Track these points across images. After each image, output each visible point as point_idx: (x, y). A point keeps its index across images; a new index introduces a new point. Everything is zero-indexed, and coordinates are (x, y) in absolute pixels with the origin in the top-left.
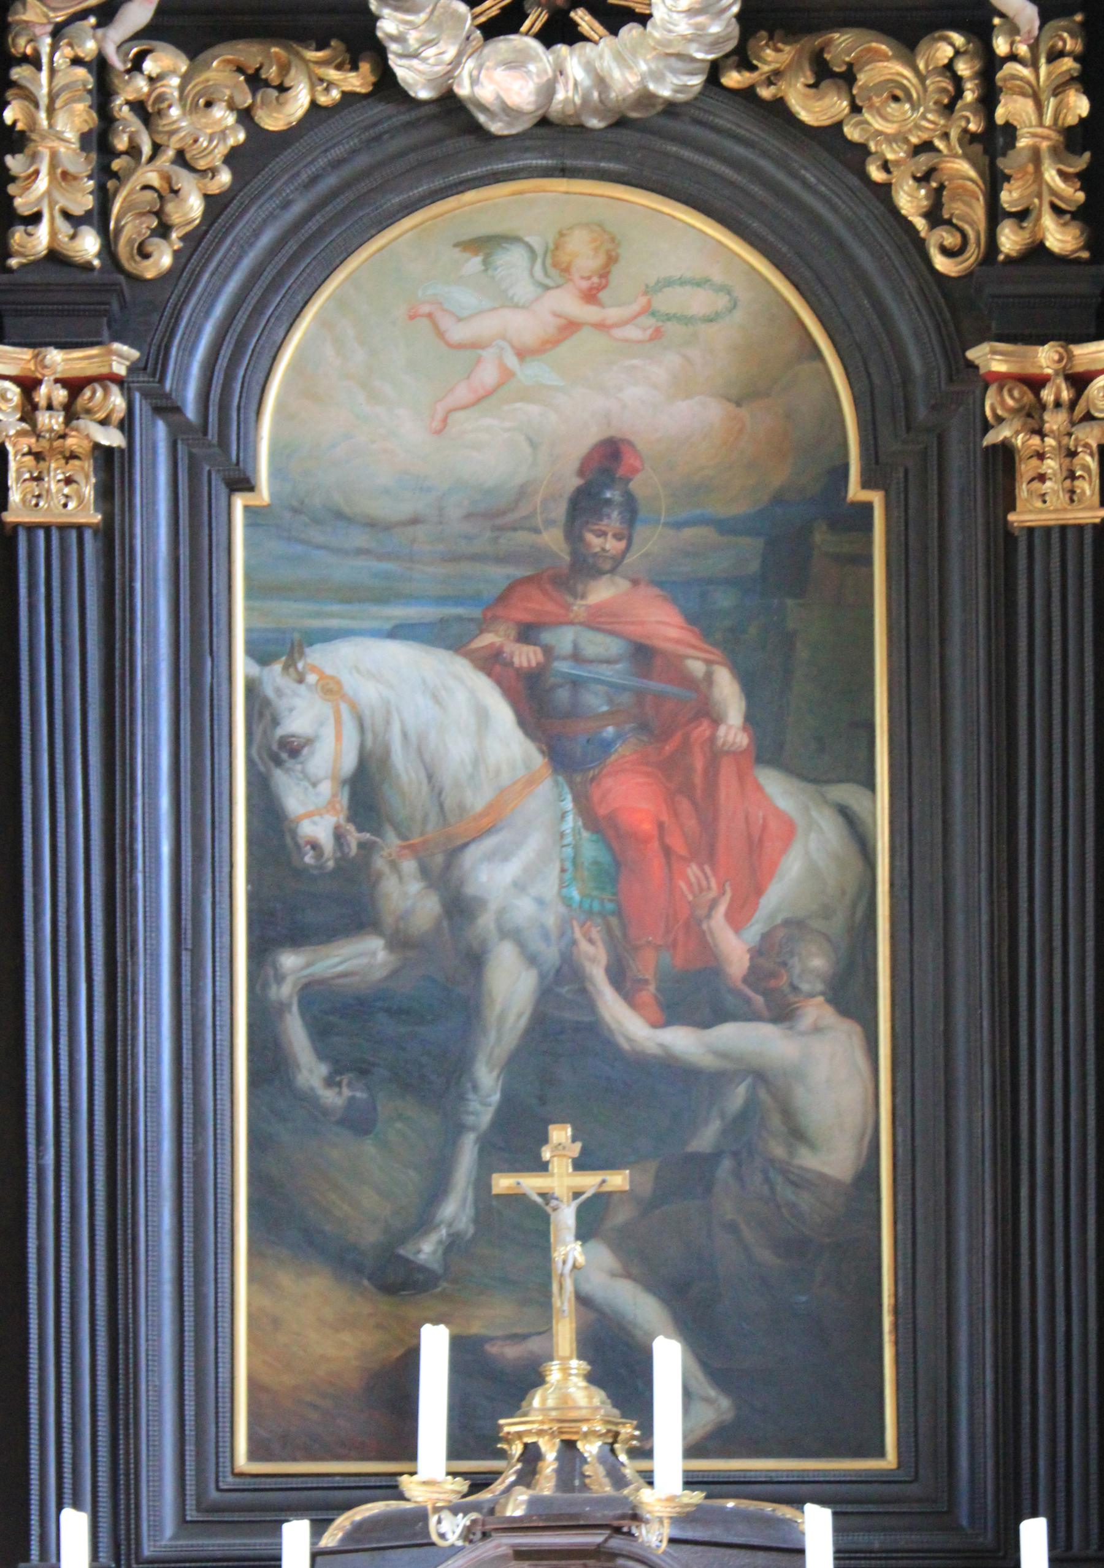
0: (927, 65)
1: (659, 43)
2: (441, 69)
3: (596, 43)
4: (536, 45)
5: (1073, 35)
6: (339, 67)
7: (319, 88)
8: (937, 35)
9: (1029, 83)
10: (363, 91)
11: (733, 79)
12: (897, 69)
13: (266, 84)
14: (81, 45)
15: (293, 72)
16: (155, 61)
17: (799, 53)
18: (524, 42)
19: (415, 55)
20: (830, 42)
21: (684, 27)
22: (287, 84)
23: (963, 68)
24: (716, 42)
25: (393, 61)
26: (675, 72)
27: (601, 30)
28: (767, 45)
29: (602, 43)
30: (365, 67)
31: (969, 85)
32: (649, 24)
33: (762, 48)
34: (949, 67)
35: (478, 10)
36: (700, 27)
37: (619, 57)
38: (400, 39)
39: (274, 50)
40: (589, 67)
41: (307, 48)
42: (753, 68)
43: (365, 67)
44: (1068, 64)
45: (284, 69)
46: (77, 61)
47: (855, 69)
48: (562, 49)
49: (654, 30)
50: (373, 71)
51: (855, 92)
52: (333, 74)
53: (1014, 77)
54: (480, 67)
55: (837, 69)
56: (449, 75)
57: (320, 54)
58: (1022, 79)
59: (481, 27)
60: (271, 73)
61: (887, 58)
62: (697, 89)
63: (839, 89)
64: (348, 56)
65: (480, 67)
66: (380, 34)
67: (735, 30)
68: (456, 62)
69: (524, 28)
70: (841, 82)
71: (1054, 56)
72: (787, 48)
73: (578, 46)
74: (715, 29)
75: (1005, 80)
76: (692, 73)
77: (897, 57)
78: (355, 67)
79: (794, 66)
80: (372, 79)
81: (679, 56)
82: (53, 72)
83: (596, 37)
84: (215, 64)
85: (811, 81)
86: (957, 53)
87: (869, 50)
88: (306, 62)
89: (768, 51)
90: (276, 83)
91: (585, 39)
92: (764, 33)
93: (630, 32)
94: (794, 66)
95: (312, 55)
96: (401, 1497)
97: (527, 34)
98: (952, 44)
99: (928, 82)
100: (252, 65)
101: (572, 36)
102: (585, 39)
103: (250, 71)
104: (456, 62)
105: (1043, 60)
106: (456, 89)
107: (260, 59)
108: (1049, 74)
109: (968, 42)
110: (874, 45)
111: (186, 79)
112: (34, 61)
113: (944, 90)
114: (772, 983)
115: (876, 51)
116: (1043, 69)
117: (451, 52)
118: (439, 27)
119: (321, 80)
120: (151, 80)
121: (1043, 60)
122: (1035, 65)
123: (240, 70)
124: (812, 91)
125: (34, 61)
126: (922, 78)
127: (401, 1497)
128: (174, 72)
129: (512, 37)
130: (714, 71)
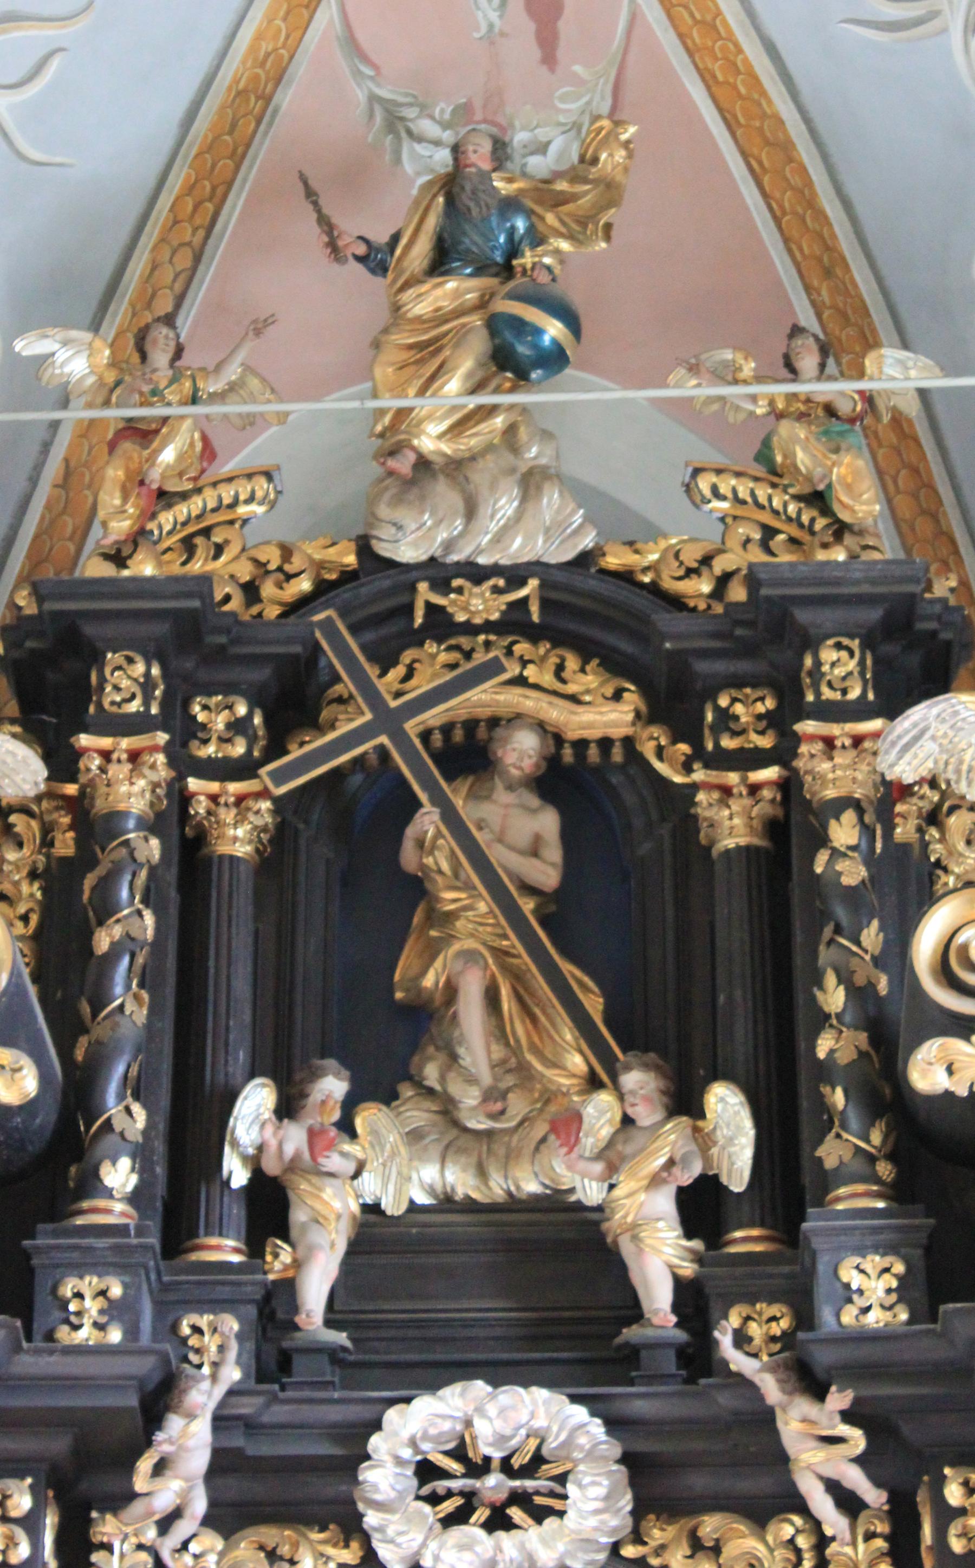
0: (775, 1540)
1: (573, 1531)
2: (411, 1551)
3: (526, 1530)
4: (481, 1533)
5: (881, 1520)
6: (335, 1545)
7: (320, 1562)
8: (782, 1516)
9: (851, 1559)
10: (353, 1563)
11: (629, 1551)
12: (752, 1544)
13: (281, 1558)
14: (144, 1534)
15: (301, 1549)
16: (199, 1542)
17: (681, 1529)
18: (472, 1531)
19: (392, 1541)
20: (703, 1521)
21: (593, 1522)
22: (296, 1559)
23: (802, 1542)
24: (615, 1530)
25: (376, 1544)
26: (586, 1551)
27: (530, 1521)
28: (654, 1526)
29: (531, 1531)
30: (355, 1545)
31: (807, 1555)
32: (565, 1517)
33: (651, 1528)
34: (792, 1541)
35: (439, 1508)
36: (603, 1522)
37: (544, 1542)
38: (381, 1529)
39: (287, 1533)
40: (522, 1547)
41: (312, 1530)
42: (645, 1543)
43: (355, 1545)
44: (880, 1543)
45: (295, 1546)
46: (140, 1547)
47: (721, 1543)
48: (501, 1534)
49: (571, 1519)
50: (362, 1547)
51: (721, 1561)
52: (330, 1551)
53: (839, 1554)
54: (440, 1548)
55: (707, 1544)
56: (418, 1553)
57: (322, 1536)
58: (845, 1555)
59: (440, 1520)
60: (285, 1550)
61: (743, 1536)
62: (602, 1562)
63: (709, 1559)
64: (342, 1537)
65: (440, 1548)
66: (365, 1526)
67: (629, 1521)
68: (424, 1545)
69: (473, 1520)
70: (711, 1554)
71: (869, 1536)
72: (670, 1528)
73: (514, 1532)
74: (614, 1522)
75: (833, 1555)
76: (598, 1551)
77: (752, 1534)
78: (347, 1546)
79: (676, 1539)
80: (360, 1554)
81: (587, 1541)
82: (122, 1556)
83: (525, 1526)
84: (242, 1545)
85: (689, 1553)
86: (798, 1531)
87: (731, 1529)
88: (310, 1542)
89: (655, 1531)
90: (288, 1557)
91: (516, 1527)
92: (652, 1517)
93: (551, 1523)
94: (676, 1539)
95: (316, 1536)
96: (488, 1158)
97: (474, 1525)
98: (792, 1523)
99: (776, 1553)
100: (270, 1545)
101: (509, 1525)
102: (516, 1527)
103: (269, 1549)
104: (424, 1545)
105: (860, 1539)
106: (422, 1563)
107: (276, 1539)
108: (865, 1551)
109: (805, 1523)
110: (735, 1525)
111: (222, 1555)
112: (108, 1547)
113: (788, 1560)
114: (496, 30)
115: (737, 1530)
116: (861, 1547)
117: (420, 1538)
118: (409, 1521)
119: (322, 1555)
120: (196, 1557)
121: (860, 1539)
122: (854, 1544)
123: (262, 1548)
124: (690, 1561)
125: (108, 1547)
126: (771, 1550)
127: (488, 1158)
128: (212, 1550)
129: (462, 1527)
130: (615, 1548)
